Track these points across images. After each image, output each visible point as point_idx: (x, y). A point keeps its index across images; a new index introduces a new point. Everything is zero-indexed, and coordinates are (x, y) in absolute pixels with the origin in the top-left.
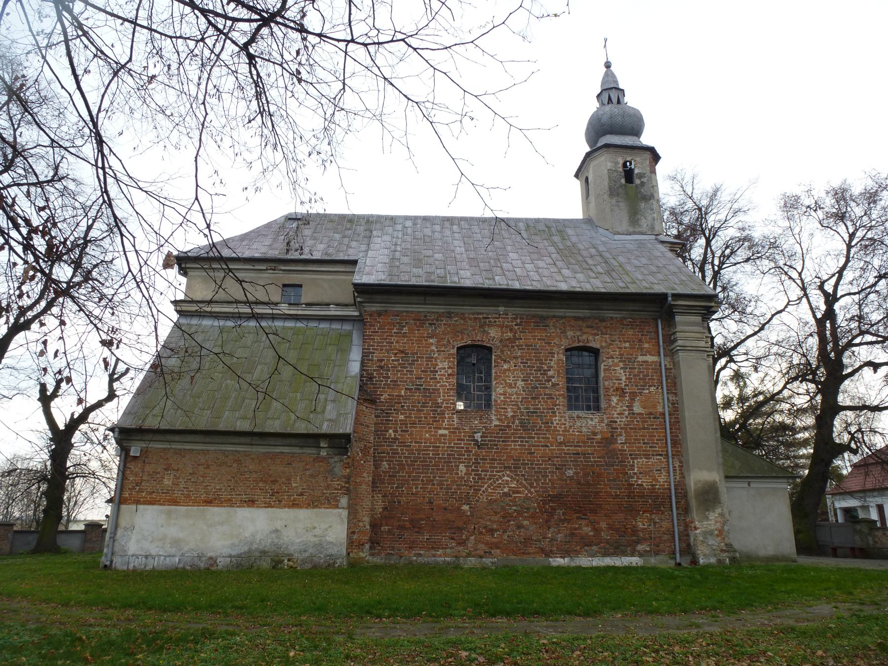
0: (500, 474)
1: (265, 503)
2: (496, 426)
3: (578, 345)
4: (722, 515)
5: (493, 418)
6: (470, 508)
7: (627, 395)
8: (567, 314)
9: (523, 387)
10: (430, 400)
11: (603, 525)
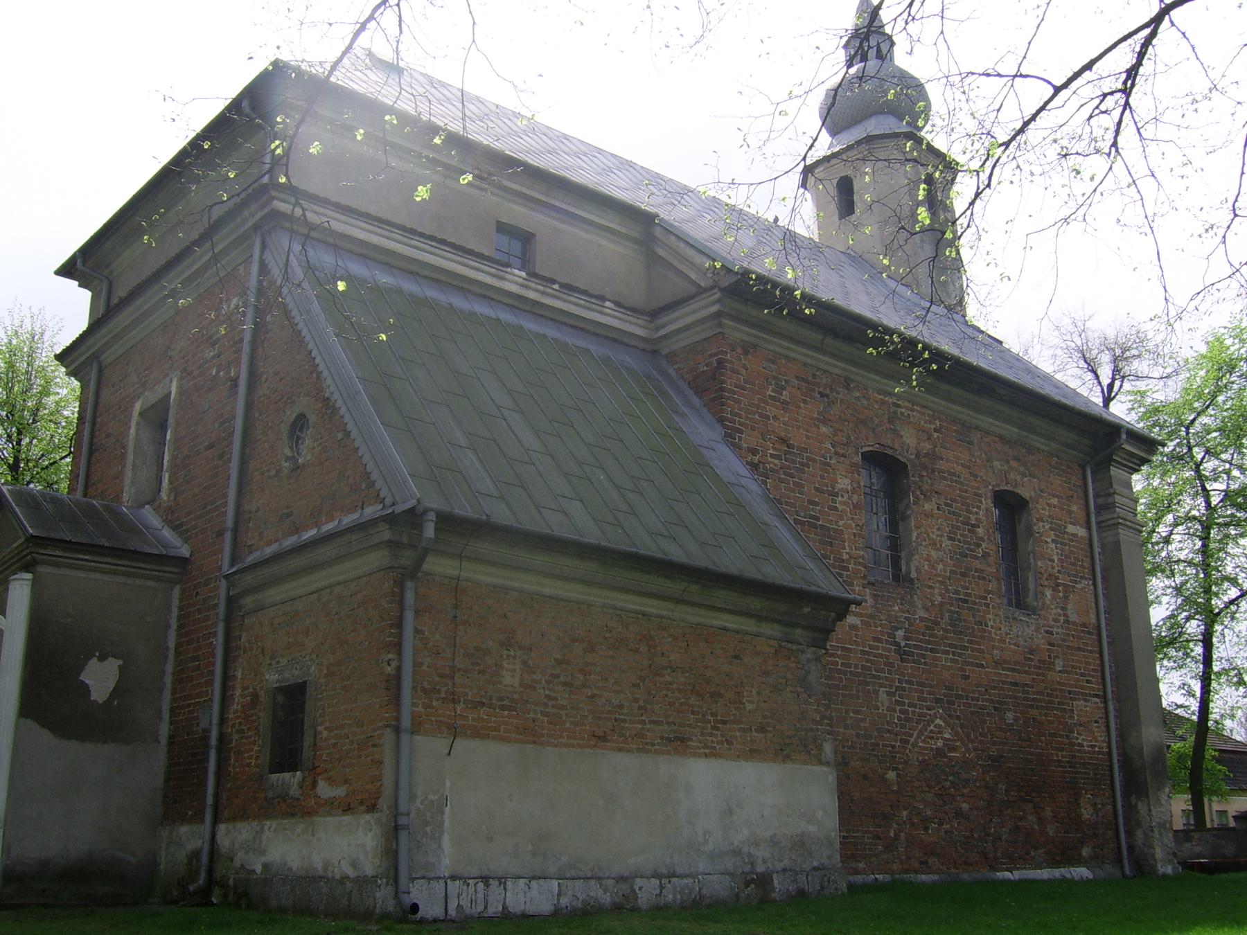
0: (932, 712)
1: (706, 747)
2: (922, 619)
3: (1006, 488)
4: (1194, 696)
5: (919, 603)
6: (898, 776)
7: (1060, 588)
8: (993, 428)
9: (950, 550)
10: (832, 552)
11: (1048, 813)
